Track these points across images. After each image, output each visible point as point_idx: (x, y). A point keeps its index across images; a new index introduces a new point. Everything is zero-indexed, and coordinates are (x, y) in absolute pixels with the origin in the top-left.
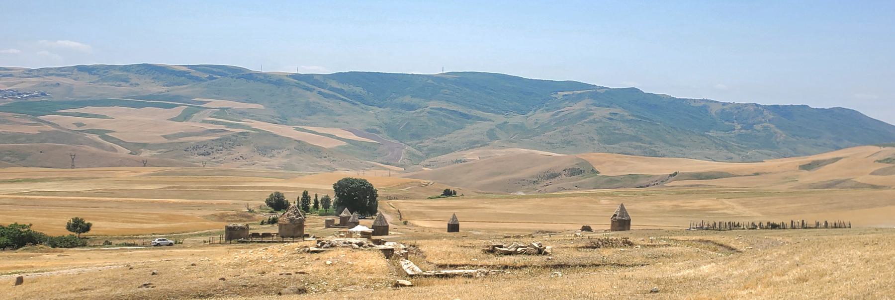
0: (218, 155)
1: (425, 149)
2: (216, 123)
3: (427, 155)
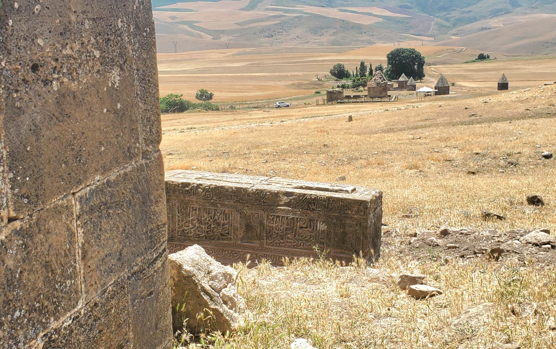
0: (279, 36)
1: (452, 19)
2: (276, 10)
3: (455, 25)
